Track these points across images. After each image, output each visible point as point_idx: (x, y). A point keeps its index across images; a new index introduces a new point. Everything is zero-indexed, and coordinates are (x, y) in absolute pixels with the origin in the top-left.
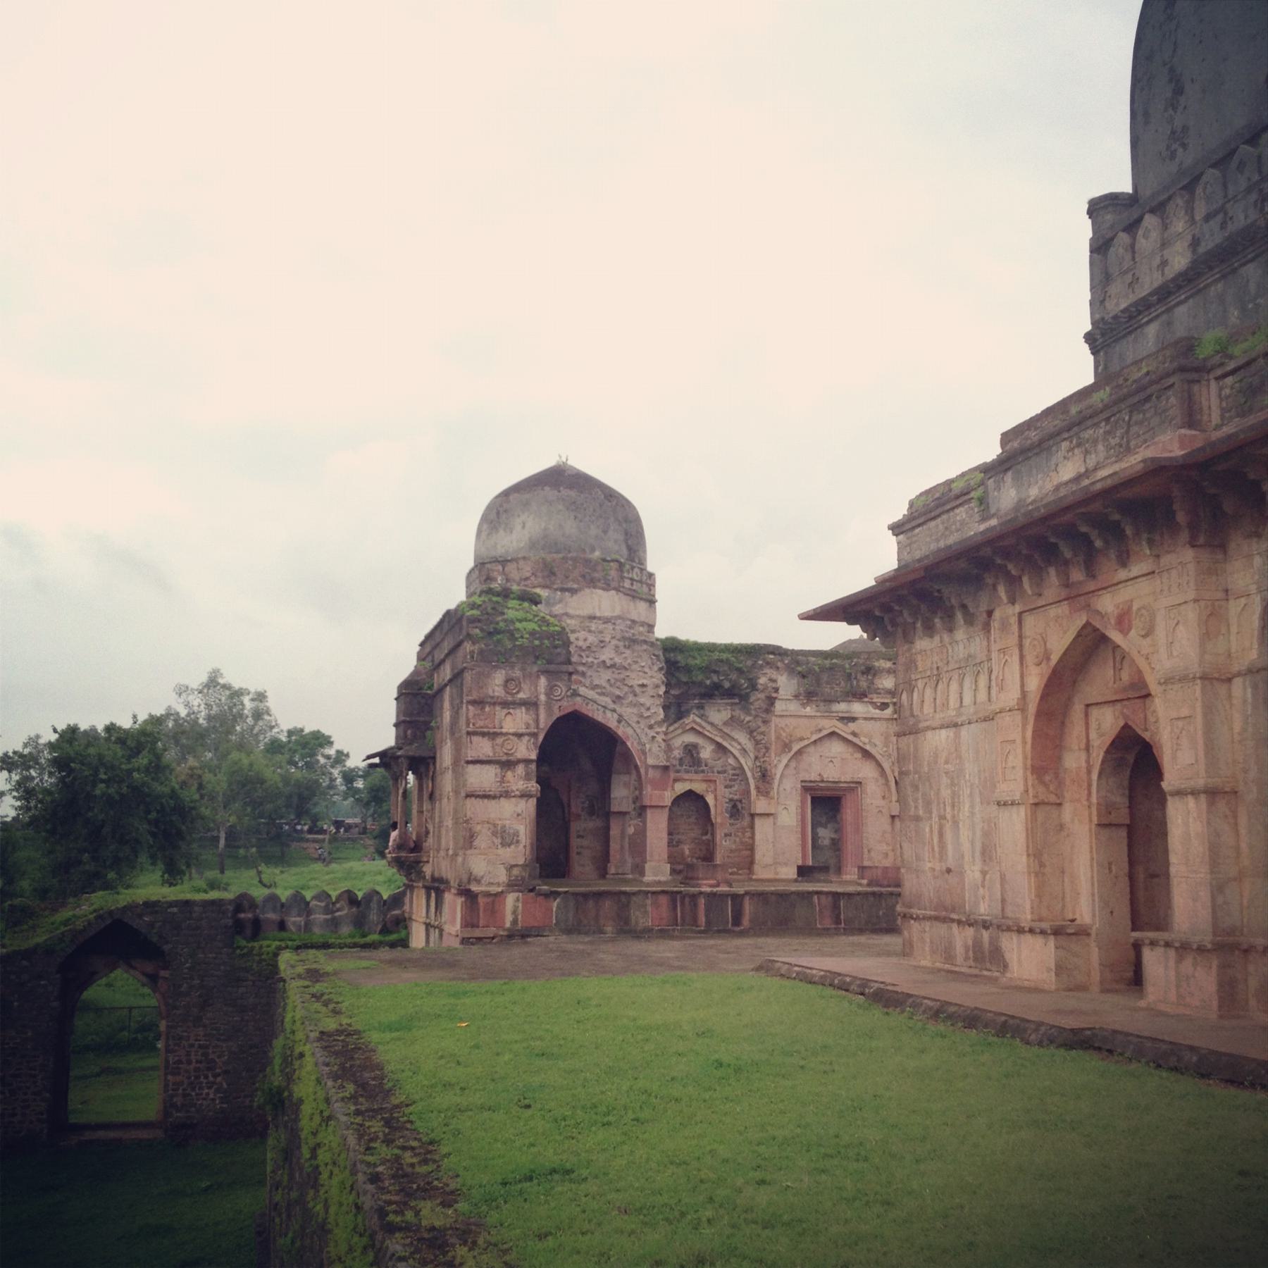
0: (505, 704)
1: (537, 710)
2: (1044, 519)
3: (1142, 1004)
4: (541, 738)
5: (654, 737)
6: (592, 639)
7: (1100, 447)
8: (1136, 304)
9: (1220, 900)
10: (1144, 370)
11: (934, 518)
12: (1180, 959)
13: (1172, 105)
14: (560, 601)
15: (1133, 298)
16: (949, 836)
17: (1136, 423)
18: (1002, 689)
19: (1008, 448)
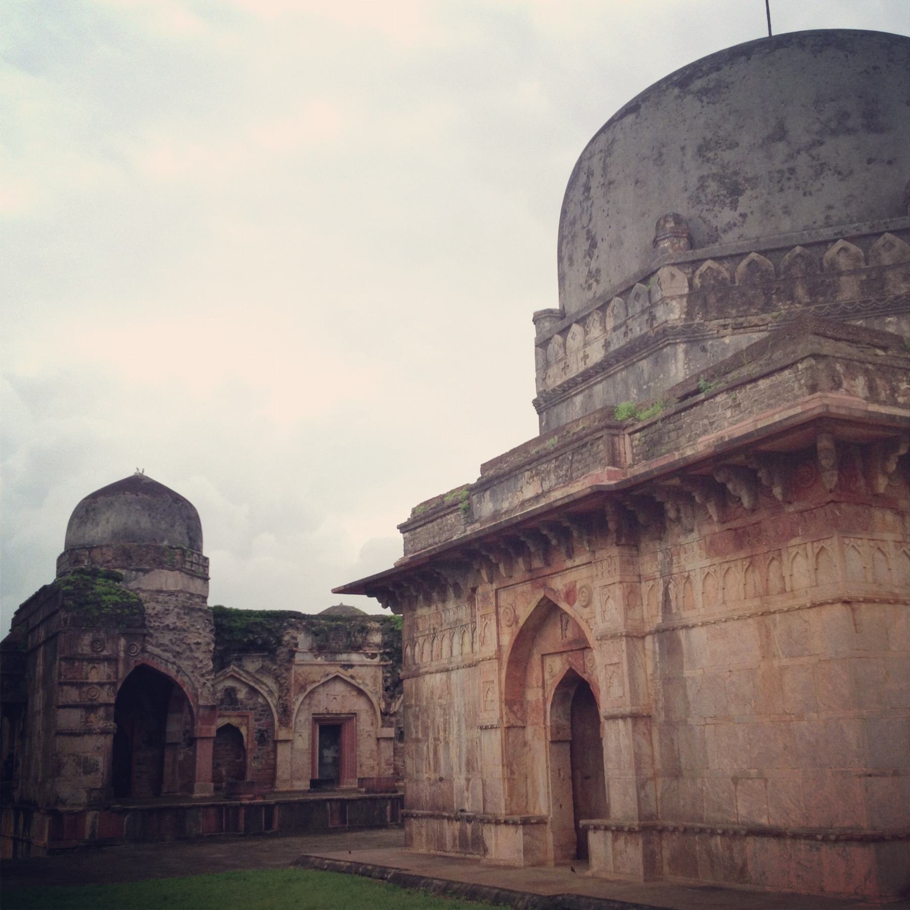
0: (91, 660)
1: (117, 664)
2: (519, 523)
3: (589, 873)
4: (119, 686)
5: (204, 684)
6: (159, 607)
7: (552, 477)
8: (568, 382)
9: (642, 794)
10: (581, 427)
11: (429, 522)
12: (615, 839)
13: (589, 255)
14: (135, 579)
16: (441, 753)
17: (576, 461)
18: (483, 643)
19: (486, 474)
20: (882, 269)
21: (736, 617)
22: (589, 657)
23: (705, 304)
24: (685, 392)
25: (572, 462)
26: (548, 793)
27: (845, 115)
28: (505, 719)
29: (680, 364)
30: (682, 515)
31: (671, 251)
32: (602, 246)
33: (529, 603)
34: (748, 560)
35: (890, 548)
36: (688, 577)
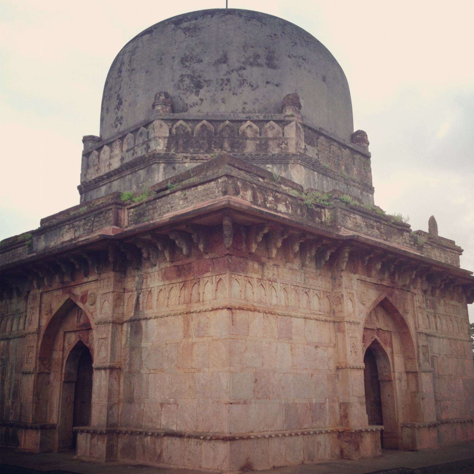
3: (75, 457)
7: (81, 229)
8: (98, 178)
10: (101, 202)
11: (7, 251)
12: (92, 437)
13: (118, 108)
15: (97, 175)
18: (30, 324)
19: (44, 225)
20: (268, 139)
21: (173, 314)
22: (91, 334)
23: (177, 143)
24: (160, 188)
25: (93, 222)
26: (59, 411)
27: (258, 56)
28: (38, 368)
29: (161, 174)
30: (151, 256)
31: (161, 112)
32: (125, 104)
33: (59, 302)
34: (183, 283)
35: (255, 282)
36: (151, 291)
